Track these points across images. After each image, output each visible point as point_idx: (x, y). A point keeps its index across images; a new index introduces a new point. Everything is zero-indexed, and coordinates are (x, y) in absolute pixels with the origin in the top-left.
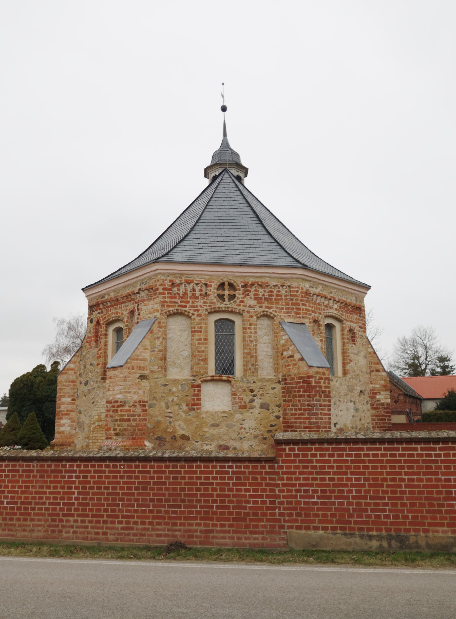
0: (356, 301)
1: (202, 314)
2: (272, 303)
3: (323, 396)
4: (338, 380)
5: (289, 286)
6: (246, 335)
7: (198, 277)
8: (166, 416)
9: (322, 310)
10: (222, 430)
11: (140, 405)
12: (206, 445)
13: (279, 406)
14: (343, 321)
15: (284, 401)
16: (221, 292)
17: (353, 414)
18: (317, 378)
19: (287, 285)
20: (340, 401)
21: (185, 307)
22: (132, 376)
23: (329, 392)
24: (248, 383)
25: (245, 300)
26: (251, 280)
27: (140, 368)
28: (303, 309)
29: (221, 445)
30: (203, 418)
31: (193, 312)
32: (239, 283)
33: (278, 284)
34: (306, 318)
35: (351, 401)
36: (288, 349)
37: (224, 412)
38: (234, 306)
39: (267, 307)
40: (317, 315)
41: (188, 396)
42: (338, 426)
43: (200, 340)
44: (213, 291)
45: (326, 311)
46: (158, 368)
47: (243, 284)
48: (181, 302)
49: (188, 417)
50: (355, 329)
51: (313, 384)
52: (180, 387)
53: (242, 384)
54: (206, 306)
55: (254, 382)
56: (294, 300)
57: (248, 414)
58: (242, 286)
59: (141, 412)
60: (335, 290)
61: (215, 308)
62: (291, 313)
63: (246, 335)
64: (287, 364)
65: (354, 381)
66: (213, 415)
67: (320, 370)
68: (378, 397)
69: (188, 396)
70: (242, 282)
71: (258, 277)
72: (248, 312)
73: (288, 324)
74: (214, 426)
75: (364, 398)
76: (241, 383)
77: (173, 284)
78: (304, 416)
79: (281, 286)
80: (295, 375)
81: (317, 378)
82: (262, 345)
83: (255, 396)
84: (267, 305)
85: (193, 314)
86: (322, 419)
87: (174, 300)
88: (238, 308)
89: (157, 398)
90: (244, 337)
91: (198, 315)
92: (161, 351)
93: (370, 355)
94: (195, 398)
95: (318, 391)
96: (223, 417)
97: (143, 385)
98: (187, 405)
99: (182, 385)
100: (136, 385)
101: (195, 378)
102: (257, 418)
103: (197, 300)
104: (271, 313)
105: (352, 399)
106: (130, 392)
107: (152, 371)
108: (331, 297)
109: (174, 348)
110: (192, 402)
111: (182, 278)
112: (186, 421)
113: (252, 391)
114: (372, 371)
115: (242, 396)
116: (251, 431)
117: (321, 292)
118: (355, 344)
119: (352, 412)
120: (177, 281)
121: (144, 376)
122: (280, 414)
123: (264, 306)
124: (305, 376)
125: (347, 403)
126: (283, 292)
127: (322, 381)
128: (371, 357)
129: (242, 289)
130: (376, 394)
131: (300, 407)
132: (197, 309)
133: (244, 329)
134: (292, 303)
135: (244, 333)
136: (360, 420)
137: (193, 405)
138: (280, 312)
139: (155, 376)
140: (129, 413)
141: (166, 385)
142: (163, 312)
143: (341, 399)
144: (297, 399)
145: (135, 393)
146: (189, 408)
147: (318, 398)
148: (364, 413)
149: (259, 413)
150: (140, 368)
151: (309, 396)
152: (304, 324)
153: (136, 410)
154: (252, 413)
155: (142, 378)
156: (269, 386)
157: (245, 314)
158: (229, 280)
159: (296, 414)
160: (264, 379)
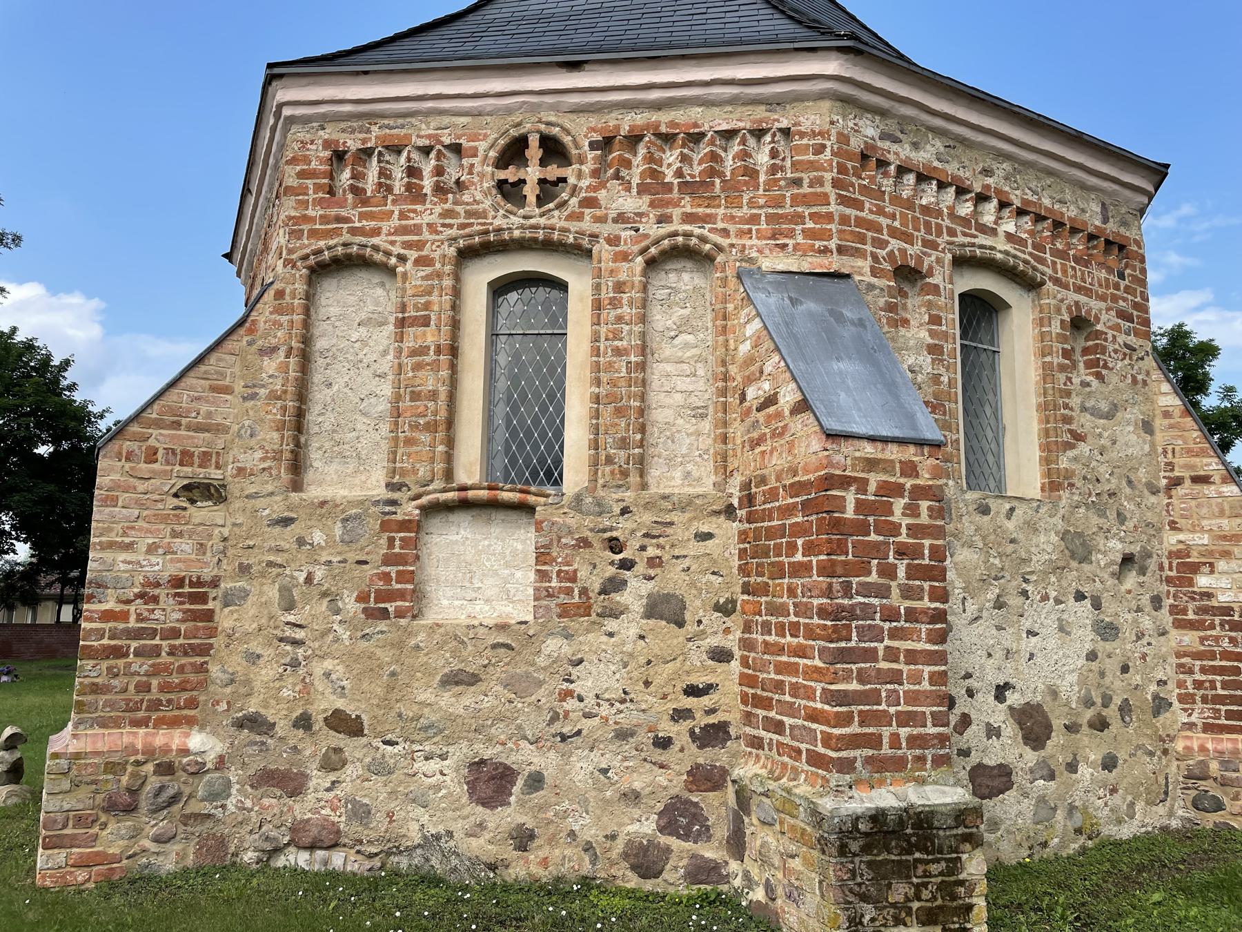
0: (1105, 220)
1: (436, 255)
2: (712, 201)
3: (901, 573)
4: (1018, 512)
5: (786, 132)
6: (603, 330)
7: (428, 124)
8: (281, 640)
9: (939, 234)
10: (489, 697)
11: (178, 594)
12: (427, 759)
13: (726, 609)
14: (1042, 283)
15: (746, 589)
16: (510, 174)
17: (1088, 646)
18: (872, 487)
19: (777, 125)
20: (1024, 593)
21: (376, 232)
22: (142, 486)
23: (938, 554)
24: (600, 514)
25: (602, 195)
26: (627, 122)
27: (186, 458)
28: (844, 220)
29: (483, 762)
30: (417, 648)
31: (402, 251)
32: (580, 133)
33: (741, 125)
34: (860, 254)
35: (1080, 596)
36: (761, 372)
37: (502, 627)
38: (557, 219)
39: (689, 218)
40: (914, 250)
41: (366, 563)
42: (1013, 698)
43: (423, 351)
44: (481, 174)
45: (961, 239)
46: (263, 459)
47: (597, 137)
48: (362, 216)
49: (364, 644)
50: (1097, 319)
51: (850, 513)
52: (338, 530)
53: (572, 520)
54: (451, 226)
55: (625, 511)
56: (806, 182)
57: (596, 639)
58: (593, 146)
59: (183, 621)
60: (1006, 165)
61: (487, 232)
62: (791, 234)
63: (603, 330)
64: (755, 435)
65: (1095, 520)
66: (456, 638)
67: (893, 453)
68: (1203, 581)
69: (366, 563)
70: (593, 130)
71: (658, 106)
72: (613, 241)
73: (770, 278)
74: (457, 683)
75: (1141, 585)
76: (572, 513)
77: (339, 156)
78: (809, 662)
79: (751, 132)
80: (778, 479)
81: (872, 487)
82: (669, 368)
83: (627, 565)
84: (688, 209)
85: (402, 259)
86: (895, 677)
87: (333, 212)
88: (574, 226)
89: (254, 569)
90: (596, 338)
91: (417, 262)
92: (279, 398)
93: (1166, 422)
94: (393, 570)
95: (878, 550)
96: (494, 646)
97: (197, 521)
98: (363, 598)
99: (345, 520)
100: (164, 519)
101: (395, 495)
102: (631, 655)
103: (419, 207)
104: (703, 239)
105: (1086, 589)
106: (129, 547)
107: (241, 470)
108: (988, 187)
109: (335, 388)
110: (380, 585)
111: (369, 131)
112: (349, 658)
113: (615, 545)
114: (1176, 482)
115: (576, 566)
116: (605, 710)
117: (936, 164)
118: (1099, 376)
119: (1085, 638)
120: (349, 143)
121: (208, 486)
122: (731, 642)
123: (676, 213)
124: (811, 477)
125: (1058, 601)
126: (762, 158)
127: (899, 504)
128: (1171, 427)
129: (591, 155)
130: (1195, 568)
131: (793, 618)
132: (416, 238)
133: (598, 306)
134: (793, 197)
135: (597, 322)
136: (1125, 669)
137: (383, 596)
138: (741, 234)
139: (252, 490)
140: (121, 626)
141: (286, 522)
142: (294, 257)
143: (1030, 588)
144: (786, 581)
145: (151, 549)
146: (365, 610)
147: (874, 577)
148: (1144, 641)
149: (642, 637)
150: (186, 458)
151: (825, 570)
152: (848, 276)
153: (158, 614)
154: (611, 635)
155: (196, 494)
156: (683, 527)
157: (602, 250)
158: (542, 127)
159: (781, 650)
160: (665, 497)
